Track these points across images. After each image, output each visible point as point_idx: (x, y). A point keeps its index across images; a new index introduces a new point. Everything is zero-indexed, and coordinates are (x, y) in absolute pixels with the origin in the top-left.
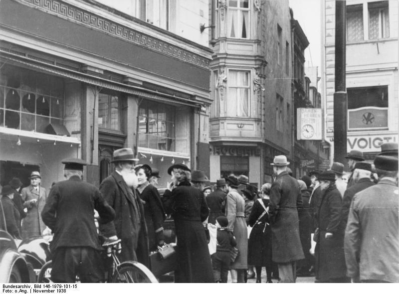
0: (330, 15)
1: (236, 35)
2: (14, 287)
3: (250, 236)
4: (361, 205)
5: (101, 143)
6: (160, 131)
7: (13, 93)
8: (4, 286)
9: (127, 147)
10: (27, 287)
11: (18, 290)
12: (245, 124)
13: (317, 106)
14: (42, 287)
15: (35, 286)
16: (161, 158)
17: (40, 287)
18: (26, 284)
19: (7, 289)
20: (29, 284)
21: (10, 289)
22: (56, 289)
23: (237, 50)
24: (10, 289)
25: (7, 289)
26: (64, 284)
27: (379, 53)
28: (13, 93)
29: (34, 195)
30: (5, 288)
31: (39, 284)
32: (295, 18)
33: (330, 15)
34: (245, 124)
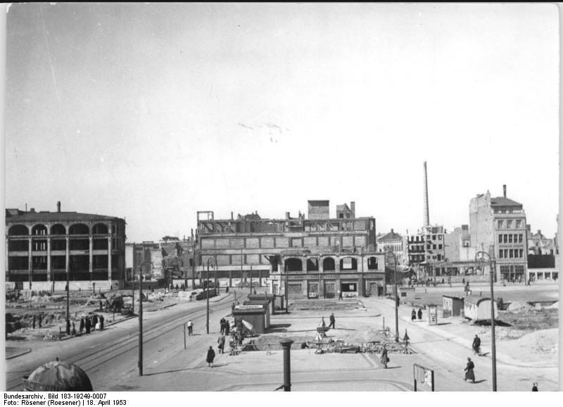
0: (317, 241)
2: (20, 397)
4: (71, 383)
6: (321, 239)
8: (5, 396)
13: (13, 344)
14: (60, 396)
15: (50, 396)
16: (10, 325)
17: (57, 397)
18: (37, 393)
19: (10, 400)
21: (13, 400)
23: (252, 254)
24: (13, 400)
25: (10, 400)
26: (75, 392)
27: (505, 186)
31: (56, 393)
33: (317, 241)
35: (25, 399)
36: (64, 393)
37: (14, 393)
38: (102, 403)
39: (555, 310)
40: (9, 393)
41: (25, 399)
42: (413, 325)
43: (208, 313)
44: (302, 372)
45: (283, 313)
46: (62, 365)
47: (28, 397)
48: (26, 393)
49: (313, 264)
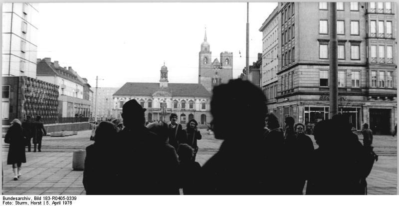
1: (152, 106)
2: (14, 199)
3: (305, 183)
5: (395, 190)
7: (360, 182)
8: (4, 198)
9: (6, 128)
10: (27, 199)
11: (14, 202)
12: (359, 47)
15: (35, 198)
18: (26, 196)
19: (7, 201)
20: (29, 196)
21: (10, 201)
22: (62, 201)
24: (10, 201)
25: (7, 201)
28: (360, 182)
29: (66, 173)
30: (5, 200)
31: (39, 196)
32: (209, 41)
34: (359, 47)
35: (18, 200)
36: (45, 196)
37: (10, 196)
38: (55, 203)
39: (3, 124)
40: (7, 196)
41: (18, 200)
42: (397, 13)
43: (30, 42)
44: (352, 101)
45: (282, 22)
46: (176, 127)
47: (19, 199)
48: (18, 196)
49: (361, 144)
